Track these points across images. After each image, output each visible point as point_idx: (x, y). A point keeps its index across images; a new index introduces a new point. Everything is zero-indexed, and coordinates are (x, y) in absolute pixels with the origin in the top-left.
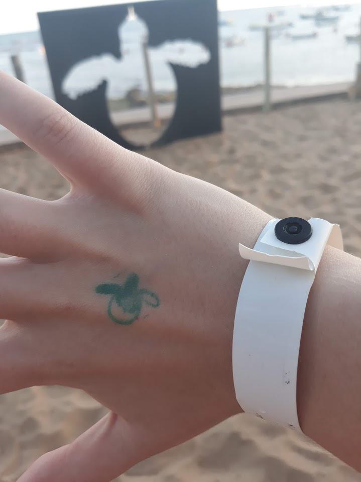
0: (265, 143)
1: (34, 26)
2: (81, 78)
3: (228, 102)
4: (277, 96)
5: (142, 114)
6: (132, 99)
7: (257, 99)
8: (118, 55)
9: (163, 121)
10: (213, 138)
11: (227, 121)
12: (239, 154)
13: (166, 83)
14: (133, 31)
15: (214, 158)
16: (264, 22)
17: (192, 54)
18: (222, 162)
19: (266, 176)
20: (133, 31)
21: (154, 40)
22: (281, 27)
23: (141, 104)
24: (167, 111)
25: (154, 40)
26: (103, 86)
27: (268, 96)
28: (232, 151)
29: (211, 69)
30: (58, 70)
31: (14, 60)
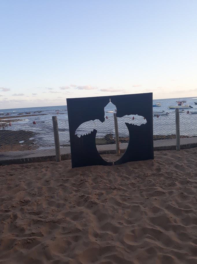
0: (177, 166)
1: (65, 104)
2: (86, 128)
3: (156, 144)
4: (183, 142)
5: (113, 147)
6: (108, 139)
7: (172, 143)
8: (102, 120)
9: (122, 151)
10: (148, 161)
11: (155, 153)
12: (163, 171)
13: (124, 131)
14: (110, 110)
15: (150, 173)
16: (177, 106)
17: (139, 120)
18: (154, 175)
19: (179, 185)
20: (110, 110)
21: (120, 114)
22: (183, 109)
23: (113, 142)
24: (124, 146)
25: (120, 114)
26: (95, 131)
27: (178, 141)
28: (159, 170)
29: (149, 126)
30: (74, 124)
31: (54, 118)
